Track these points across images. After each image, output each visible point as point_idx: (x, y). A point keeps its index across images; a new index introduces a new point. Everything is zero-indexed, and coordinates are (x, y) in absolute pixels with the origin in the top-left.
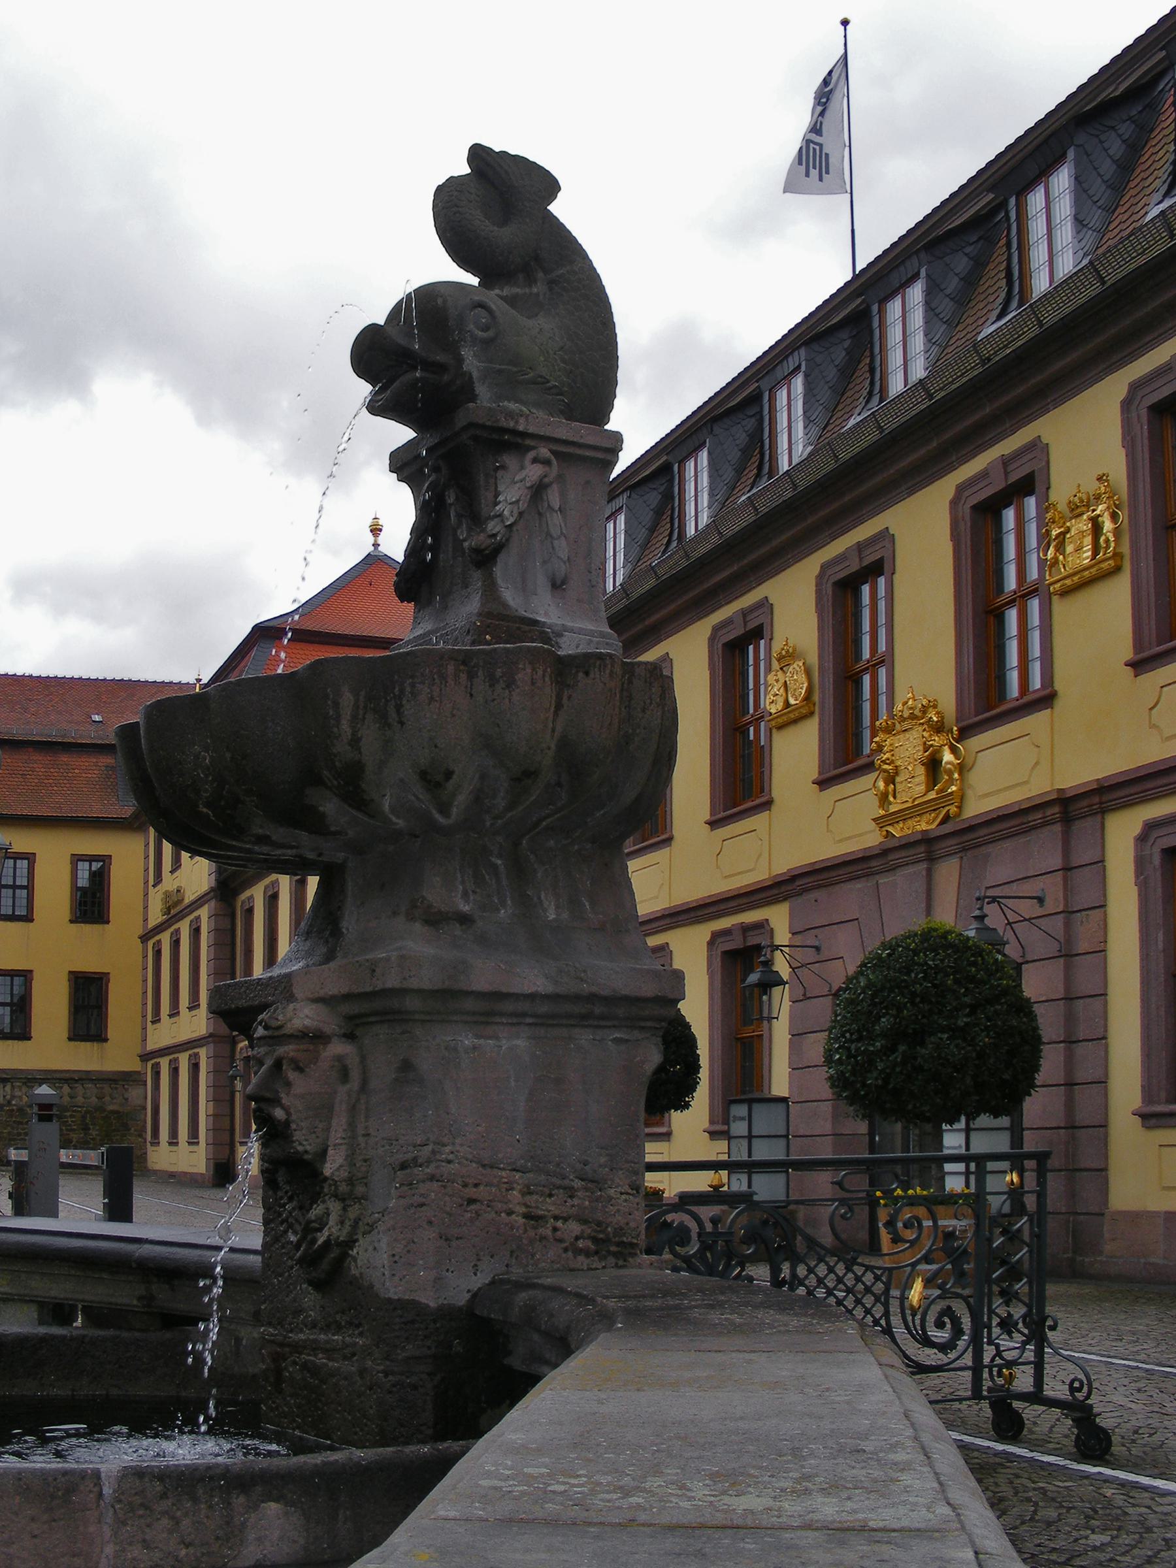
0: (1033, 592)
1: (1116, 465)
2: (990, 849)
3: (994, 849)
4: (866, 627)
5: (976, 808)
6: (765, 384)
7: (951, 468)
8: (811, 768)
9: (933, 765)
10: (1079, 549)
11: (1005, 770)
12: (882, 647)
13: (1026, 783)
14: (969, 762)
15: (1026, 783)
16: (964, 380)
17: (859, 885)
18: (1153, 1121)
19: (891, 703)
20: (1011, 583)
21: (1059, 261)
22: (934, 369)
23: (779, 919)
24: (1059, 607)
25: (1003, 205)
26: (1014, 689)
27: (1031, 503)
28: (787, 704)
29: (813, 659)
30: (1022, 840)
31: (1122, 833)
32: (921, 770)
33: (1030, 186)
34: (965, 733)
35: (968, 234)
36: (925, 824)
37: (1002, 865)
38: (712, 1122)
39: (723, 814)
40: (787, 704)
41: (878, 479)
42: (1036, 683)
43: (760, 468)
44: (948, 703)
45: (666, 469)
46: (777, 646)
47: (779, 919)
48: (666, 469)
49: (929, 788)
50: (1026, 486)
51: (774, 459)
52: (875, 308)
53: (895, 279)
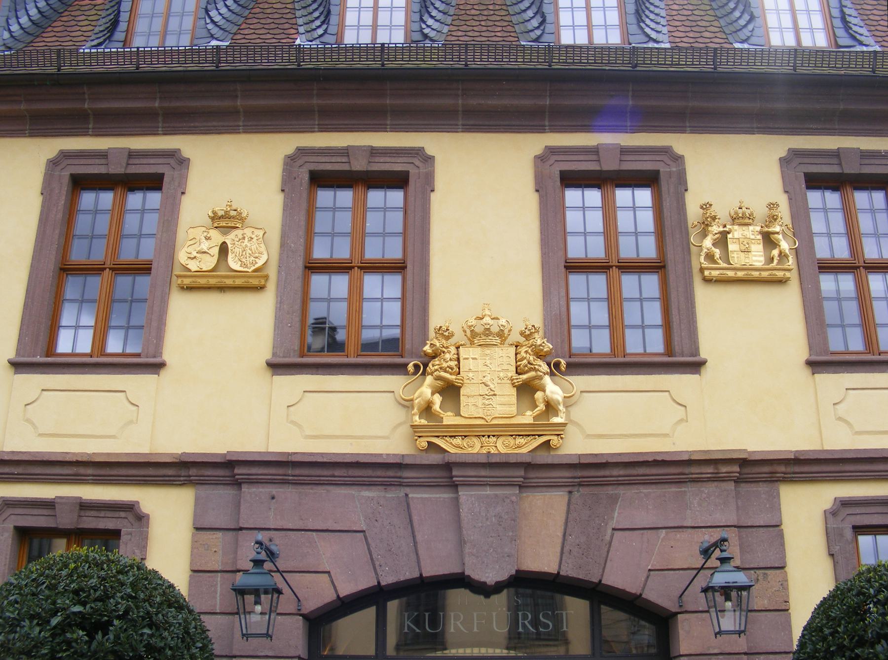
2: (621, 490)
11: (609, 418)
15: (113, 437)
30: (674, 489)
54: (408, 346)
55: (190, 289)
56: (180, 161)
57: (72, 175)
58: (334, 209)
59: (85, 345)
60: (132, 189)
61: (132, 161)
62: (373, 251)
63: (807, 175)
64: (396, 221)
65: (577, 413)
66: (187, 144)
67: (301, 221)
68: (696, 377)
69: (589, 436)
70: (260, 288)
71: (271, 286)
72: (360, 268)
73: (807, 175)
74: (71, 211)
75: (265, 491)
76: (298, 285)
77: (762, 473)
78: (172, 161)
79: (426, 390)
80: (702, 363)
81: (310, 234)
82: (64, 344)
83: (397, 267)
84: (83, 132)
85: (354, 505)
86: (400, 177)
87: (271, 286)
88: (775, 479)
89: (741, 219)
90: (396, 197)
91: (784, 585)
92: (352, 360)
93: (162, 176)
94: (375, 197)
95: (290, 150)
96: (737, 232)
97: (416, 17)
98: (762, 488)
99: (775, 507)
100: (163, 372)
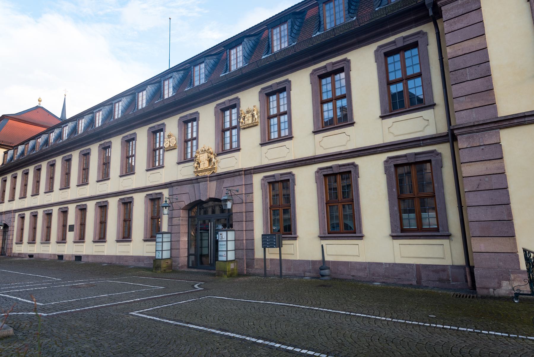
0: (161, 148)
1: (258, 104)
2: (225, 179)
3: (225, 180)
4: (131, 149)
5: (219, 171)
6: (162, 79)
7: (216, 100)
8: (176, 160)
9: (210, 161)
10: (248, 120)
11: (226, 164)
12: (134, 153)
13: (344, 145)
14: (219, 161)
15: (344, 145)
16: (374, 20)
17: (189, 186)
18: (395, 238)
19: (197, 148)
20: (158, 146)
21: (238, 64)
22: (122, 117)
23: (166, 193)
24: (242, 132)
25: (190, 67)
26: (157, 165)
27: (162, 133)
28: (170, 146)
29: (177, 137)
30: (233, 178)
31: (257, 179)
32: (208, 162)
33: (140, 92)
34: (218, 155)
35: (186, 69)
36: (207, 174)
37: (227, 183)
38: (392, 232)
39: (388, 114)
40: (170, 146)
41: (198, 100)
42: (161, 164)
43: (227, 68)
44: (213, 150)
45: (160, 82)
46: (167, 134)
47: (166, 193)
48: (304, 11)
49: (209, 165)
50: (161, 130)
51: (95, 124)
52: (192, 67)
53: (198, 62)
54: (426, 101)
55: (244, 129)
56: (197, 113)
57: (318, 76)
58: (412, 57)
59: (276, 136)
60: (336, 74)
61: (405, 40)
62: (409, 72)
63: (266, 94)
64: (416, 60)
65: (220, 165)
66: (240, 95)
67: (265, 105)
68: (352, 127)
69: (325, 149)
70: (257, 125)
71: (259, 124)
72: (406, 79)
73: (266, 94)
74: (321, 86)
75: (177, 187)
76: (386, 89)
77: (250, 172)
78: (420, 35)
79: (196, 165)
80: (354, 123)
81: (321, 93)
82: (283, 134)
83: (419, 75)
84: (101, 141)
85: (187, 188)
86: (343, 68)
87: (259, 124)
88: (251, 174)
89: (248, 112)
90: (415, 51)
91: (252, 197)
92: (336, 126)
93: (417, 42)
94: (408, 54)
95: (179, 118)
96: (247, 115)
97: (347, 12)
98: (249, 176)
99: (252, 180)
100: (355, 125)
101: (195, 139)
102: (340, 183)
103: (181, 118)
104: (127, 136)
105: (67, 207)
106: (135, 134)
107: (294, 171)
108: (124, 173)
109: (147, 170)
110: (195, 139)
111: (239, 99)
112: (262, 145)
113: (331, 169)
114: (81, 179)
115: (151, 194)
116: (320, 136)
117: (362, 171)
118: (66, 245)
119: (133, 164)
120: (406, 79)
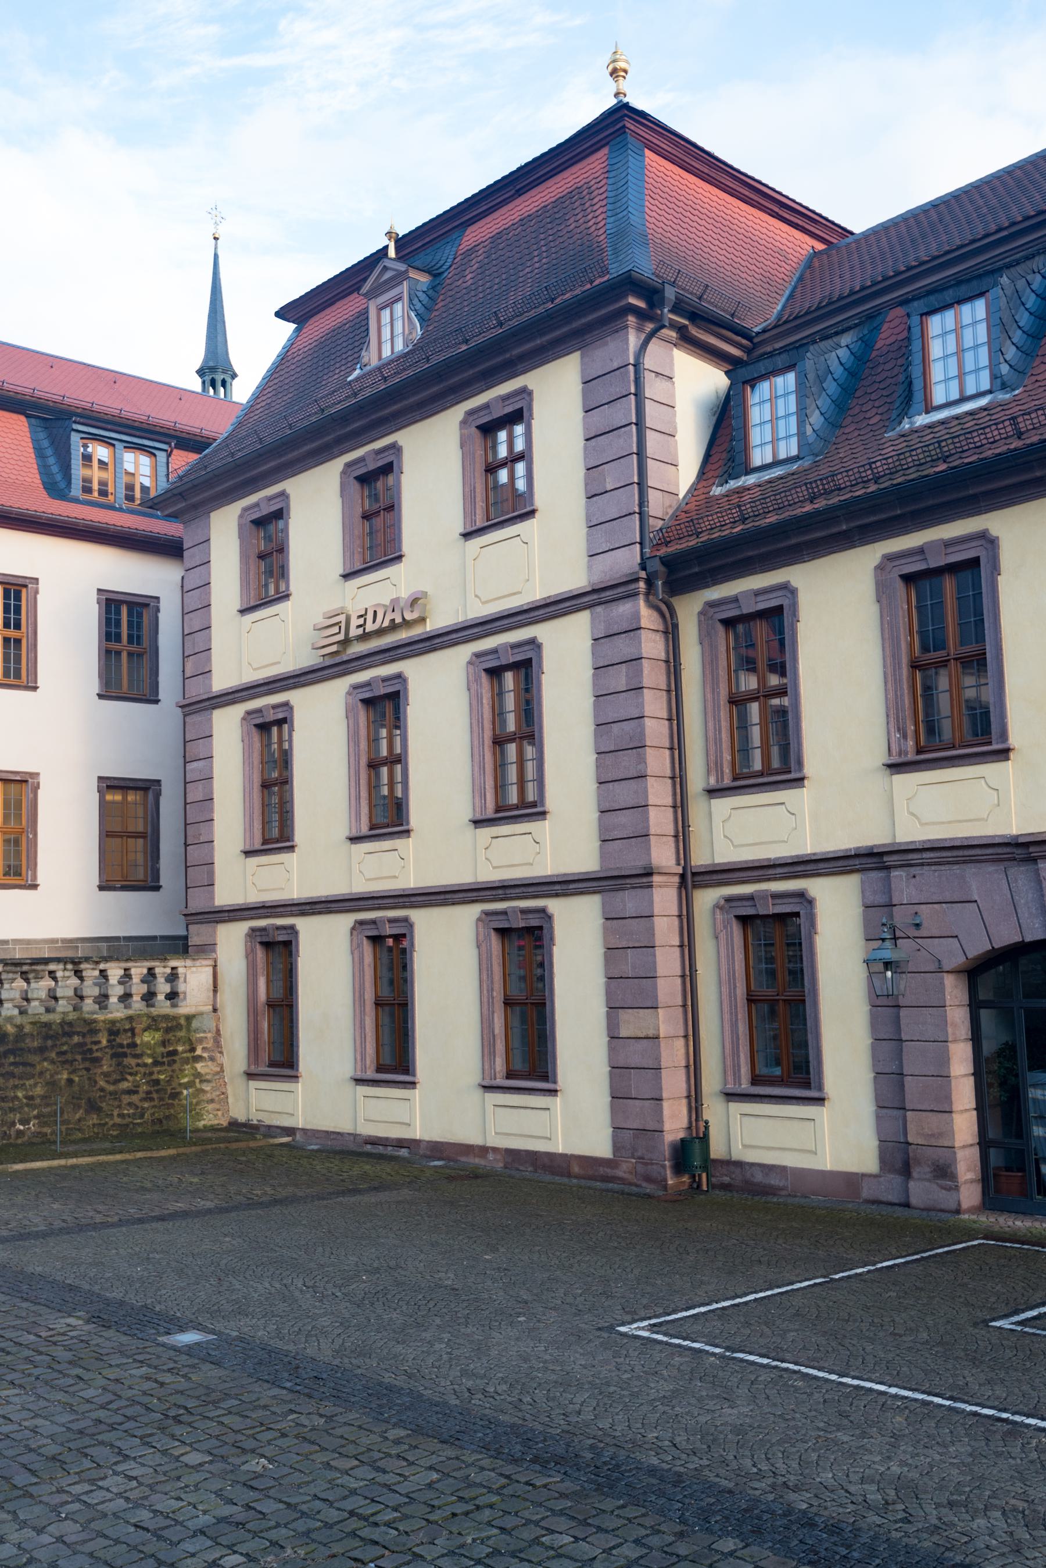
7: (342, 453)
72: (512, 461)
101: (521, 457)
102: (761, 631)
103: (470, 413)
104: (486, 406)
105: (399, 677)
106: (525, 393)
107: (554, 906)
108: (365, 830)
109: (467, 536)
110: (521, 457)
111: (530, 394)
112: (242, 612)
113: (260, 715)
114: (480, 505)
115: (259, 711)
116: (486, 833)
117: (300, 718)
118: (417, 1093)
119: (521, 485)
120: (512, 461)
